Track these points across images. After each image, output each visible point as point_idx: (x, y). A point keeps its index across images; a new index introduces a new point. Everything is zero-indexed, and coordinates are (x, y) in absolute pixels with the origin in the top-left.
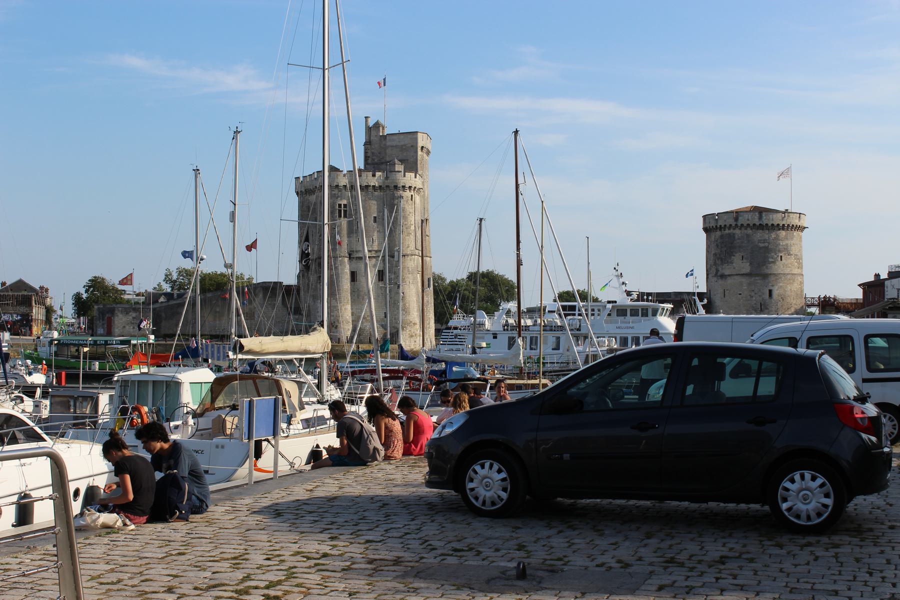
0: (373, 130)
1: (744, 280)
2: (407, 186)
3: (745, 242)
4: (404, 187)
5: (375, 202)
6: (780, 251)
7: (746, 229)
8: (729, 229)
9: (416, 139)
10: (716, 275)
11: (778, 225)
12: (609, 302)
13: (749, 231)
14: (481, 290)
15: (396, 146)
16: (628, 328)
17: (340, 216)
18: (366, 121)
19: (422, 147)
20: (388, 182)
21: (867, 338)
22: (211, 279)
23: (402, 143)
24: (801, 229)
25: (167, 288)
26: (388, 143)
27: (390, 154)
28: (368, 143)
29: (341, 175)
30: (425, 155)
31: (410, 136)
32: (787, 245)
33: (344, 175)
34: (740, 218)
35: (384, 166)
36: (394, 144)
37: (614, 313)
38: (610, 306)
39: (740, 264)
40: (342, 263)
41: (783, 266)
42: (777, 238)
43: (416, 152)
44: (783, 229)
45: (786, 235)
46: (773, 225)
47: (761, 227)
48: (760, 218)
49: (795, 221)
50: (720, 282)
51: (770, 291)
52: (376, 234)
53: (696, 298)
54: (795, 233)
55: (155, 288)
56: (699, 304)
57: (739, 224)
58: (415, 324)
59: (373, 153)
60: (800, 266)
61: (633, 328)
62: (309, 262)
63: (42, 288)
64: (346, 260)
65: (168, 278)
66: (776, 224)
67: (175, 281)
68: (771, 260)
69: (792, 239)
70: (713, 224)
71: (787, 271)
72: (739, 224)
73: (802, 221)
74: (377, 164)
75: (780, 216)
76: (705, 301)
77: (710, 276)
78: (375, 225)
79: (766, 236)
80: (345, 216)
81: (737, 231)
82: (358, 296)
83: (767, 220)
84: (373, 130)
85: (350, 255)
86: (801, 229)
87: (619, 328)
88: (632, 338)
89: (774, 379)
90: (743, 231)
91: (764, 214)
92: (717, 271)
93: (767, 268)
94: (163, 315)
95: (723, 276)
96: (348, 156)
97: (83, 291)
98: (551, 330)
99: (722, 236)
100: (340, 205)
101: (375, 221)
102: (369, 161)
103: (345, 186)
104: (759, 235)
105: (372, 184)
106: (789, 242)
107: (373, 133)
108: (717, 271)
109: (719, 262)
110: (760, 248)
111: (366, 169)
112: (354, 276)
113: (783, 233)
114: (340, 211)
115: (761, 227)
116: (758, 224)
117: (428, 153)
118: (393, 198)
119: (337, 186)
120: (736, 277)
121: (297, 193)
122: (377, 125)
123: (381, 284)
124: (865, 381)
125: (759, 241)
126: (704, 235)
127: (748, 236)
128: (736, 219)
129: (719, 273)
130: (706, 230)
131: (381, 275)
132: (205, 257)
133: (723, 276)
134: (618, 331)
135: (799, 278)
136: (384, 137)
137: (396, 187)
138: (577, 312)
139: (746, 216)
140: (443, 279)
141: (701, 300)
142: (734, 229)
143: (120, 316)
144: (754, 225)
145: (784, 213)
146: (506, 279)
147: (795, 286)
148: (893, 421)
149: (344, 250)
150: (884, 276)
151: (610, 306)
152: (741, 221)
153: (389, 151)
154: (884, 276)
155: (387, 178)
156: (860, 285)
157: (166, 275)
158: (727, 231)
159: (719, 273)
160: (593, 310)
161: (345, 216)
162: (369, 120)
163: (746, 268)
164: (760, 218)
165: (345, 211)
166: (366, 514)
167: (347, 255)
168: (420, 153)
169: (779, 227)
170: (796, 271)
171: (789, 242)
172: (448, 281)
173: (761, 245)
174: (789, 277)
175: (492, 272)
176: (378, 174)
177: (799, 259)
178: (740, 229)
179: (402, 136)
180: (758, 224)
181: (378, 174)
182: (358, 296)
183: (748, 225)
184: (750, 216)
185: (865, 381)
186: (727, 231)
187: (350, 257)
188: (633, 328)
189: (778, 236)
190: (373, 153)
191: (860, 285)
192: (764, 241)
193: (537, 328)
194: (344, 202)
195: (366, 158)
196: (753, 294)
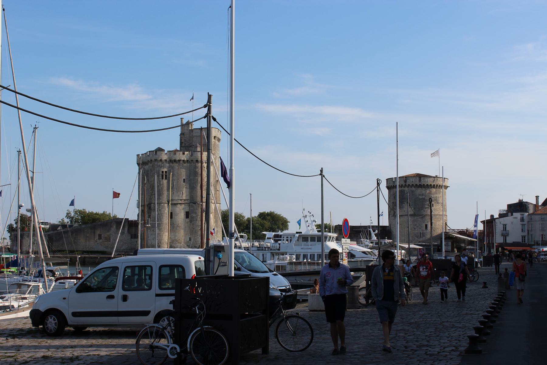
3: (413, 194)
5: (184, 170)
7: (411, 187)
12: (297, 233)
13: (413, 189)
14: (267, 224)
16: (307, 249)
17: (163, 178)
18: (181, 121)
19: (215, 137)
20: (192, 158)
21: (161, 267)
22: (89, 216)
24: (446, 187)
25: (66, 220)
26: (194, 134)
27: (196, 140)
29: (163, 153)
30: (217, 142)
33: (166, 154)
34: (408, 181)
35: (191, 148)
37: (301, 239)
38: (297, 235)
40: (164, 207)
41: (436, 209)
42: (430, 193)
44: (434, 188)
45: (436, 191)
46: (427, 185)
47: (421, 186)
48: (420, 181)
49: (440, 182)
52: (184, 189)
53: (371, 230)
55: (60, 222)
56: (373, 234)
57: (407, 185)
59: (185, 140)
60: (444, 209)
61: (311, 249)
62: (147, 206)
64: (166, 205)
65: (68, 215)
66: (429, 184)
67: (73, 218)
70: (392, 184)
72: (407, 185)
73: (445, 183)
74: (187, 147)
75: (432, 179)
76: (377, 231)
78: (184, 184)
79: (424, 192)
80: (166, 178)
81: (406, 189)
82: (173, 227)
83: (424, 182)
86: (446, 187)
87: (302, 249)
88: (310, 255)
90: (410, 188)
91: (422, 178)
93: (424, 211)
94: (54, 239)
96: (171, 142)
97: (13, 223)
98: (262, 250)
100: (163, 172)
101: (184, 181)
102: (183, 145)
103: (166, 160)
104: (419, 191)
105: (183, 159)
106: (437, 195)
111: (181, 150)
112: (171, 216)
113: (434, 190)
114: (163, 176)
115: (421, 186)
116: (418, 184)
117: (219, 140)
119: (161, 160)
121: (138, 164)
123: (188, 220)
124: (157, 295)
125: (420, 195)
126: (387, 191)
127: (412, 192)
128: (405, 181)
131: (187, 215)
132: (23, 205)
134: (303, 251)
136: (192, 130)
138: (282, 239)
139: (411, 179)
140: (243, 217)
141: (374, 231)
142: (404, 187)
144: (416, 185)
145: (434, 177)
146: (282, 217)
148: (164, 320)
150: (496, 216)
151: (297, 235)
152: (409, 182)
153: (194, 139)
154: (496, 216)
155: (192, 155)
157: (67, 214)
160: (287, 237)
161: (166, 178)
164: (420, 181)
165: (166, 176)
168: (213, 140)
169: (440, 187)
171: (437, 195)
172: (246, 218)
173: (421, 197)
174: (438, 216)
175: (273, 212)
176: (186, 153)
177: (444, 206)
178: (408, 187)
180: (418, 184)
181: (186, 153)
182: (173, 227)
183: (413, 185)
184: (413, 179)
185: (157, 295)
188: (311, 249)
189: (431, 191)
190: (185, 140)
192: (423, 195)
193: (253, 249)
194: (165, 170)
195: (181, 143)
196: (416, 227)
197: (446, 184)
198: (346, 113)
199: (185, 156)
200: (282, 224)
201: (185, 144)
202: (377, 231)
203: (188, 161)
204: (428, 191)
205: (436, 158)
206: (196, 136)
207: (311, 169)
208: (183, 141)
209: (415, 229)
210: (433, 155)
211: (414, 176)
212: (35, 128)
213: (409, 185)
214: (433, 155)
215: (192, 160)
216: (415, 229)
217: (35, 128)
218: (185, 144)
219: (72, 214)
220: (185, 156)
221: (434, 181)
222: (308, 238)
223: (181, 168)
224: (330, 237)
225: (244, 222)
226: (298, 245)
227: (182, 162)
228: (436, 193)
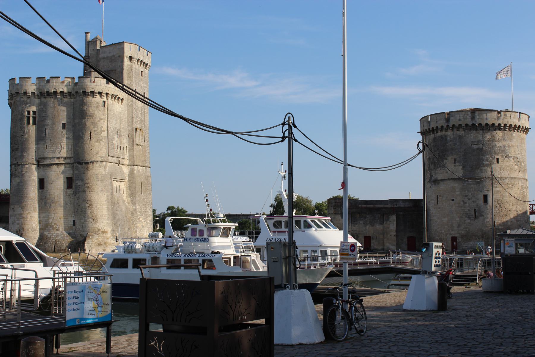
1: (457, 185)
2: (104, 92)
4: (93, 93)
5: (64, 108)
6: (496, 153)
7: (458, 130)
8: (441, 131)
9: (122, 49)
10: (430, 181)
11: (493, 124)
13: (462, 132)
15: (107, 58)
17: (29, 123)
23: (112, 54)
26: (101, 56)
31: (118, 47)
32: (504, 146)
34: (451, 118)
36: (105, 55)
39: (453, 167)
41: (502, 168)
42: (492, 139)
43: (122, 62)
44: (500, 129)
46: (487, 125)
47: (474, 127)
49: (513, 120)
50: (434, 188)
51: (486, 197)
54: (515, 134)
58: (104, 232)
60: (522, 169)
63: (168, 209)
64: (34, 167)
66: (490, 123)
68: (485, 163)
69: (511, 140)
71: (505, 174)
72: (451, 125)
77: (426, 181)
78: (64, 132)
79: (480, 137)
81: (449, 133)
82: (45, 203)
85: (38, 162)
89: (138, 334)
90: (456, 132)
92: (431, 176)
93: (482, 172)
95: (436, 182)
99: (435, 139)
103: (33, 93)
104: (472, 136)
105: (60, 90)
106: (506, 143)
108: (431, 176)
109: (432, 167)
110: (474, 150)
112: (42, 183)
115: (474, 127)
116: (470, 124)
118: (83, 104)
119: (25, 93)
120: (448, 182)
122: (94, 41)
123: (70, 191)
125: (473, 143)
127: (460, 137)
128: (448, 120)
129: (433, 179)
130: (422, 133)
131: (69, 183)
133: (436, 182)
135: (521, 183)
137: (85, 93)
139: (458, 116)
142: (446, 130)
144: (467, 125)
147: (515, 191)
149: (31, 154)
158: (439, 134)
159: (433, 179)
162: (89, 35)
163: (459, 171)
164: (473, 118)
165: (34, 118)
166: (528, 336)
167: (35, 162)
168: (126, 62)
170: (516, 175)
171: (506, 143)
174: (507, 181)
178: (452, 130)
179: (111, 48)
180: (470, 124)
182: (46, 203)
183: (460, 125)
186: (439, 134)
187: (39, 165)
194: (34, 108)
196: (466, 200)
203: (70, 93)
204: (488, 136)
206: (104, 58)
209: (465, 203)
213: (454, 125)
216: (465, 203)
221: (498, 118)
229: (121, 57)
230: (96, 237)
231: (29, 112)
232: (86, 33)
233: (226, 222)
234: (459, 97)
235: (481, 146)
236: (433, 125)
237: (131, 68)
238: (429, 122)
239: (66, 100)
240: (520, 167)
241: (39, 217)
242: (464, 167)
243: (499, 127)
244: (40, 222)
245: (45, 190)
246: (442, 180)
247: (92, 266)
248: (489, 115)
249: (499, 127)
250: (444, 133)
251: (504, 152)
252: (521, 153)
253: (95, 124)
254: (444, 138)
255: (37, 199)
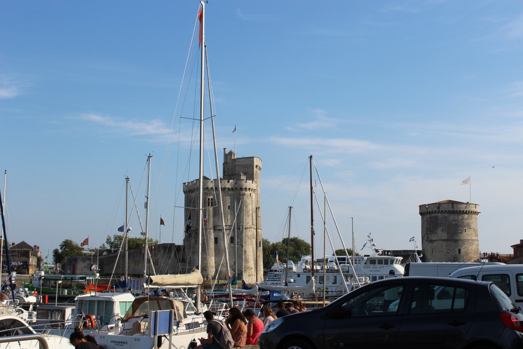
0: (228, 156)
1: (444, 243)
3: (444, 221)
4: (246, 189)
5: (229, 197)
6: (464, 226)
7: (444, 213)
9: (253, 161)
10: (427, 240)
11: (463, 211)
12: (365, 256)
13: (446, 215)
16: (376, 271)
17: (209, 205)
18: (224, 151)
19: (257, 166)
21: (517, 275)
24: (477, 213)
25: (108, 247)
26: (237, 164)
28: (225, 164)
29: (210, 181)
30: (258, 170)
31: (249, 159)
32: (468, 223)
33: (212, 182)
36: (240, 164)
38: (366, 258)
39: (441, 234)
42: (463, 219)
43: (253, 168)
44: (466, 213)
45: (468, 217)
46: (460, 211)
47: (453, 212)
48: (453, 207)
49: (473, 209)
50: (430, 244)
51: (459, 250)
52: (229, 216)
53: (416, 253)
54: (473, 216)
56: (418, 257)
57: (440, 210)
58: (252, 268)
59: (228, 169)
60: (476, 235)
61: (379, 271)
62: (191, 231)
64: (212, 231)
65: (108, 241)
66: (462, 210)
67: (112, 243)
69: (471, 219)
70: (425, 211)
71: (469, 238)
72: (440, 210)
73: (477, 209)
75: (464, 206)
76: (422, 255)
77: (424, 241)
78: (229, 210)
79: (456, 218)
81: (439, 215)
82: (219, 252)
84: (228, 156)
85: (214, 228)
86: (477, 213)
91: (455, 205)
92: (428, 238)
95: (431, 241)
96: (214, 171)
97: (59, 248)
99: (430, 218)
102: (226, 174)
103: (212, 188)
104: (452, 217)
105: (228, 187)
106: (469, 221)
107: (228, 157)
108: (428, 238)
109: (429, 233)
112: (216, 240)
113: (466, 216)
114: (209, 202)
115: (453, 212)
118: (240, 195)
122: (231, 153)
125: (453, 220)
126: (420, 217)
127: (446, 217)
128: (439, 208)
129: (429, 239)
131: (232, 240)
132: (131, 228)
133: (431, 241)
134: (371, 273)
135: (476, 242)
136: (235, 160)
138: (346, 262)
139: (444, 206)
140: (268, 243)
141: (419, 255)
142: (438, 213)
143: (80, 263)
144: (449, 211)
145: (466, 204)
147: (474, 247)
151: (366, 258)
153: (237, 168)
155: (236, 183)
156: (512, 246)
157: (108, 239)
158: (433, 215)
159: (429, 239)
160: (356, 260)
161: (212, 205)
162: (226, 150)
163: (445, 236)
164: (453, 207)
165: (212, 203)
168: (255, 169)
170: (474, 238)
171: (469, 221)
172: (271, 243)
173: (454, 223)
174: (470, 241)
175: (297, 238)
176: (231, 181)
177: (475, 231)
178: (441, 213)
179: (245, 160)
182: (219, 252)
186: (433, 215)
187: (215, 229)
188: (379, 271)
189: (463, 217)
190: (228, 169)
191: (512, 246)
194: (211, 197)
196: (449, 251)
197: (478, 210)
198: (356, 146)
199: (229, 184)
200: (306, 249)
201: (228, 173)
202: (422, 255)
203: (232, 188)
204: (460, 217)
205: (467, 185)
206: (239, 165)
207: (351, 198)
208: (226, 170)
209: (448, 253)
210: (465, 182)
211: (447, 203)
212: (149, 157)
213: (442, 211)
214: (465, 182)
215: (236, 188)
216: (448, 253)
217: (149, 157)
218: (228, 173)
219: (112, 240)
220: (229, 184)
221: (466, 207)
222: (375, 261)
223: (226, 195)
224: (397, 260)
225: (269, 248)
226: (367, 268)
227: (227, 190)
228: (468, 219)
229: (252, 165)
230: (248, 271)
231: (209, 199)
232: (224, 149)
233: (183, 288)
234: (440, 191)
235: (456, 222)
236: (429, 210)
237: (257, 171)
238: (427, 208)
239: (230, 192)
240: (476, 233)
241: (215, 259)
242: (448, 234)
243: (466, 213)
244: (215, 262)
245: (218, 244)
246: (435, 240)
247: (348, 263)
248: (461, 206)
249: (466, 213)
250: (436, 214)
251: (468, 225)
252: (476, 226)
253: (247, 206)
254: (436, 217)
255: (214, 249)
